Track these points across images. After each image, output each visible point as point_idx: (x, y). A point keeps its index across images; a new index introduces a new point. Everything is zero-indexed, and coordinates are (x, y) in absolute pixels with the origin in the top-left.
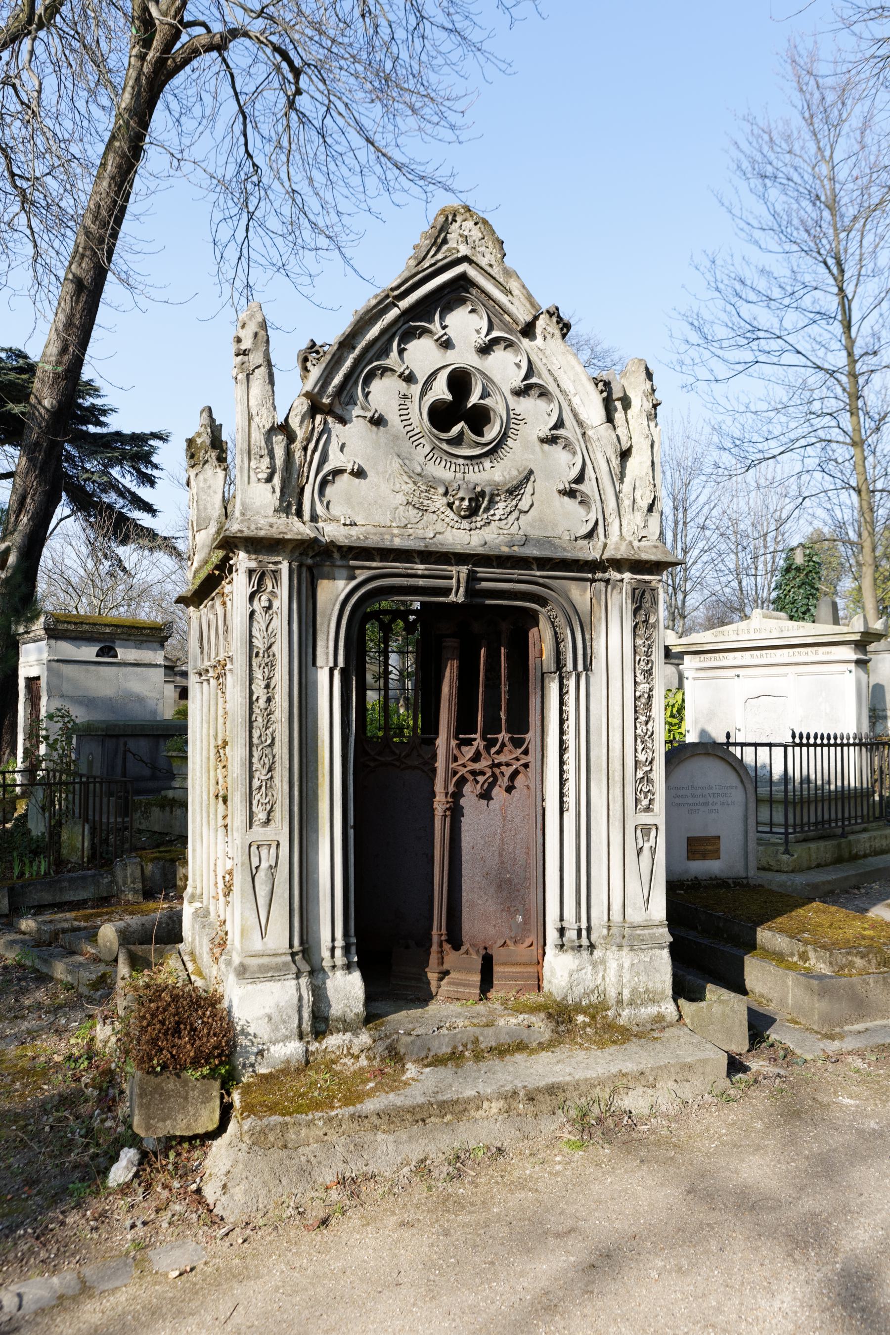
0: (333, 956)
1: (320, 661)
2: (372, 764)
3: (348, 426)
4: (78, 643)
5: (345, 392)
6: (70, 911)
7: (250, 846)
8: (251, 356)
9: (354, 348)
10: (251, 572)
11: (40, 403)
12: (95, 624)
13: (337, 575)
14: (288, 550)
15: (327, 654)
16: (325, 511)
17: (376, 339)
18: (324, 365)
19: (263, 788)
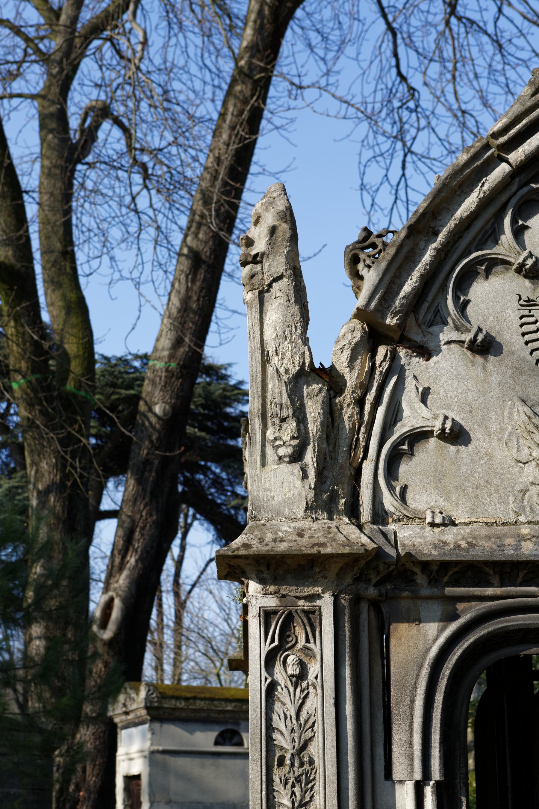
1: (398, 772)
3: (434, 359)
4: (191, 726)
5: (425, 305)
8: (266, 264)
9: (436, 234)
10: (267, 616)
11: (150, 410)
12: (212, 699)
13: (423, 614)
15: (411, 757)
16: (398, 504)
17: (474, 216)
18: (384, 264)
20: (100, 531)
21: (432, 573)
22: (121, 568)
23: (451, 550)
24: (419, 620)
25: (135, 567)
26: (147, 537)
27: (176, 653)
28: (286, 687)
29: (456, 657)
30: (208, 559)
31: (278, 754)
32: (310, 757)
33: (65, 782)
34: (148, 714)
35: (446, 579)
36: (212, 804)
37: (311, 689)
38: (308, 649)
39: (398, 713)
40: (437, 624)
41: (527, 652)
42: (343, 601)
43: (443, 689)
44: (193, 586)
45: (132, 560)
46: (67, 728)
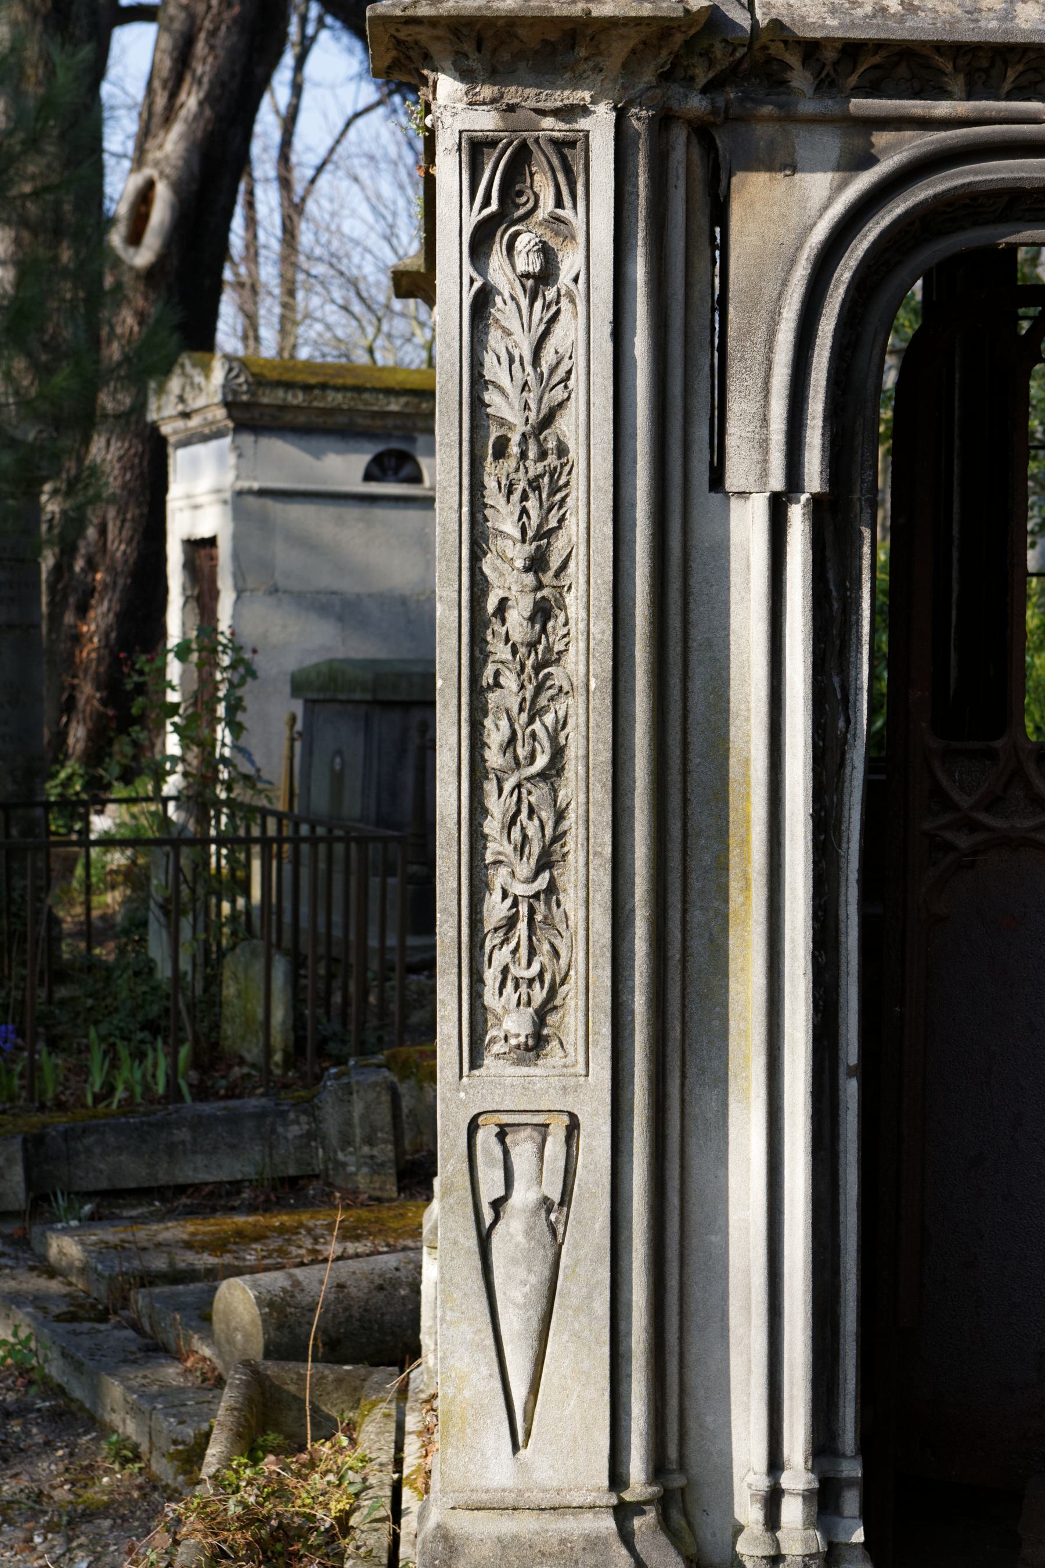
0: (772, 1521)
1: (734, 480)
2: (963, 841)
4: (315, 442)
6: (190, 1212)
7: (473, 1127)
10: (476, 149)
12: (359, 389)
13: (802, 153)
14: (614, 62)
15: (764, 446)
19: (522, 926)
20: (123, 51)
21: (824, 65)
22: (168, 120)
23: (867, 16)
24: (792, 167)
25: (197, 117)
26: (221, 53)
27: (284, 305)
28: (513, 298)
29: (865, 245)
30: (350, 112)
31: (494, 433)
32: (559, 440)
33: (67, 552)
34: (230, 416)
35: (853, 80)
36: (358, 596)
37: (564, 303)
38: (558, 219)
39: (742, 357)
40: (829, 175)
41: (1012, 239)
42: (635, 122)
43: (836, 311)
44: (320, 169)
45: (190, 101)
46: (67, 442)
